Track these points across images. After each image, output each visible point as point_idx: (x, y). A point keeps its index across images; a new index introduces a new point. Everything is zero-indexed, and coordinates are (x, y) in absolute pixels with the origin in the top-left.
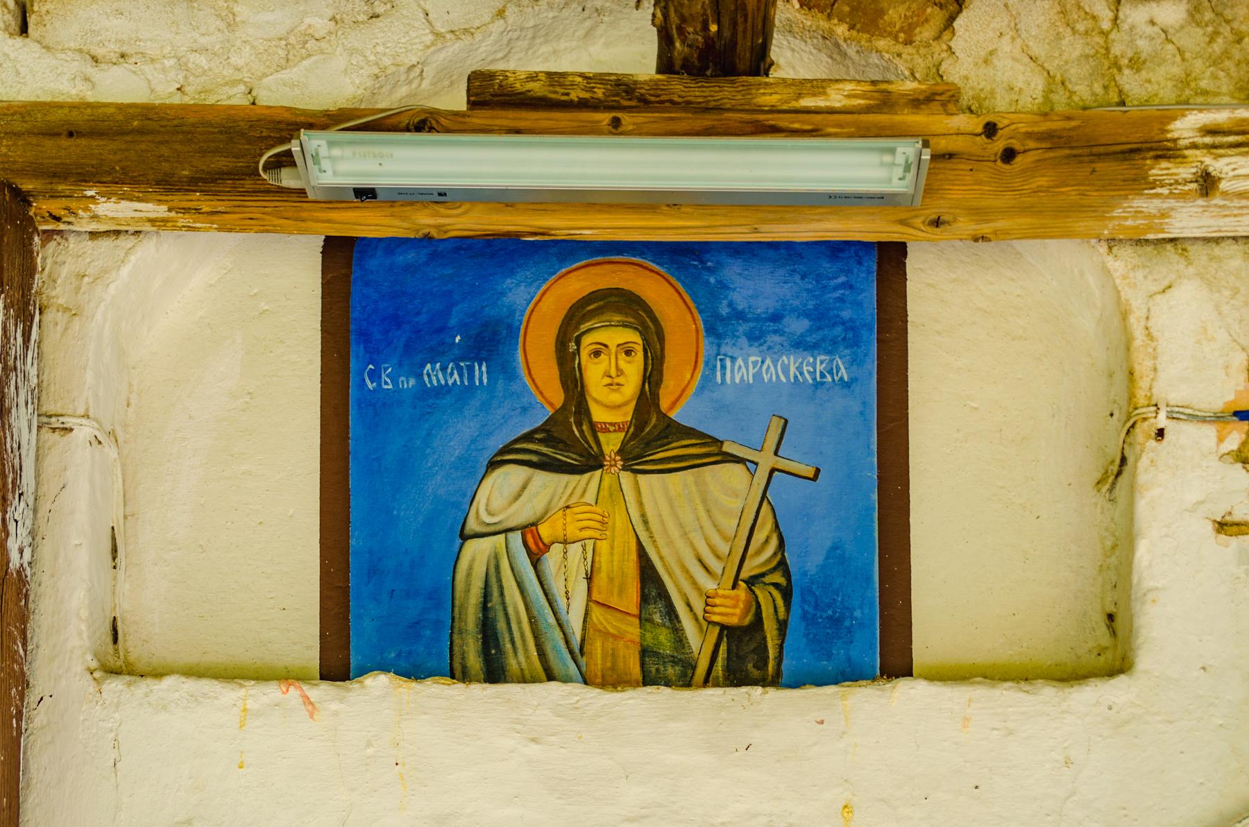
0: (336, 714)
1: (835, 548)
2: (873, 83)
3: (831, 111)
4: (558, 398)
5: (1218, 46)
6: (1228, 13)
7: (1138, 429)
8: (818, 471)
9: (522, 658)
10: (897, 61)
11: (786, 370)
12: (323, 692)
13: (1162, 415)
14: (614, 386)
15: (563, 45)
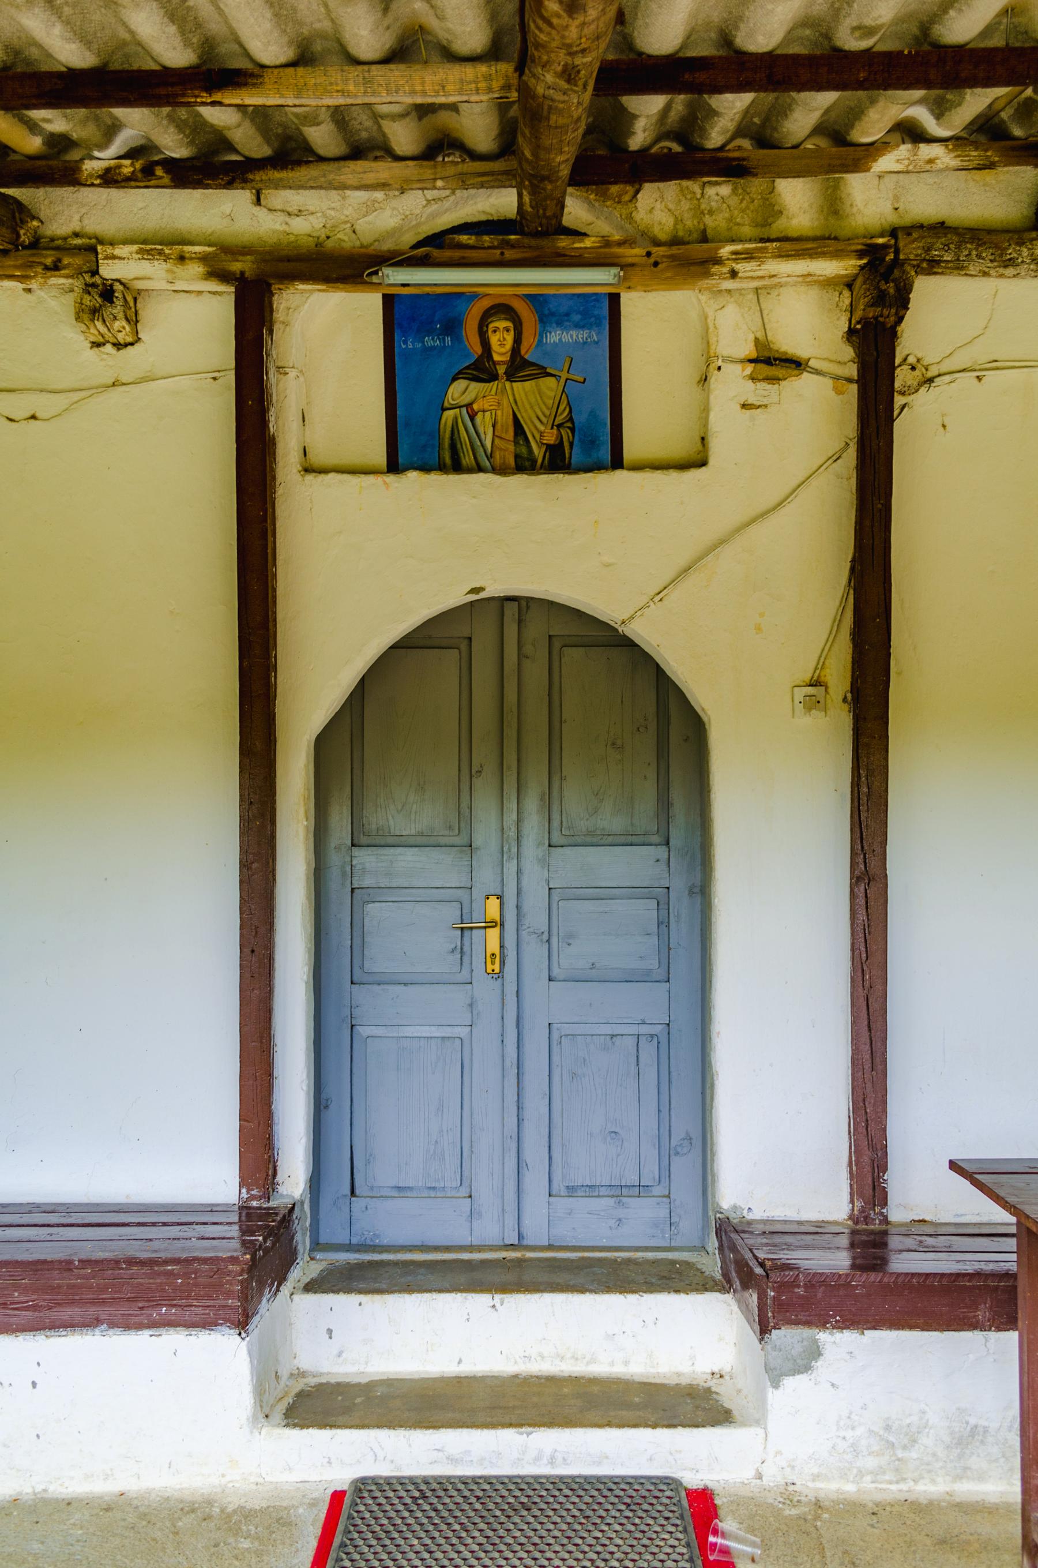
0: (396, 488)
1: (592, 412)
2: (603, 237)
3: (586, 248)
4: (479, 350)
5: (744, 205)
6: (748, 190)
7: (711, 366)
8: (585, 379)
9: (467, 460)
10: (615, 211)
11: (572, 337)
12: (391, 478)
13: (720, 360)
14: (502, 345)
15: (479, 199)
